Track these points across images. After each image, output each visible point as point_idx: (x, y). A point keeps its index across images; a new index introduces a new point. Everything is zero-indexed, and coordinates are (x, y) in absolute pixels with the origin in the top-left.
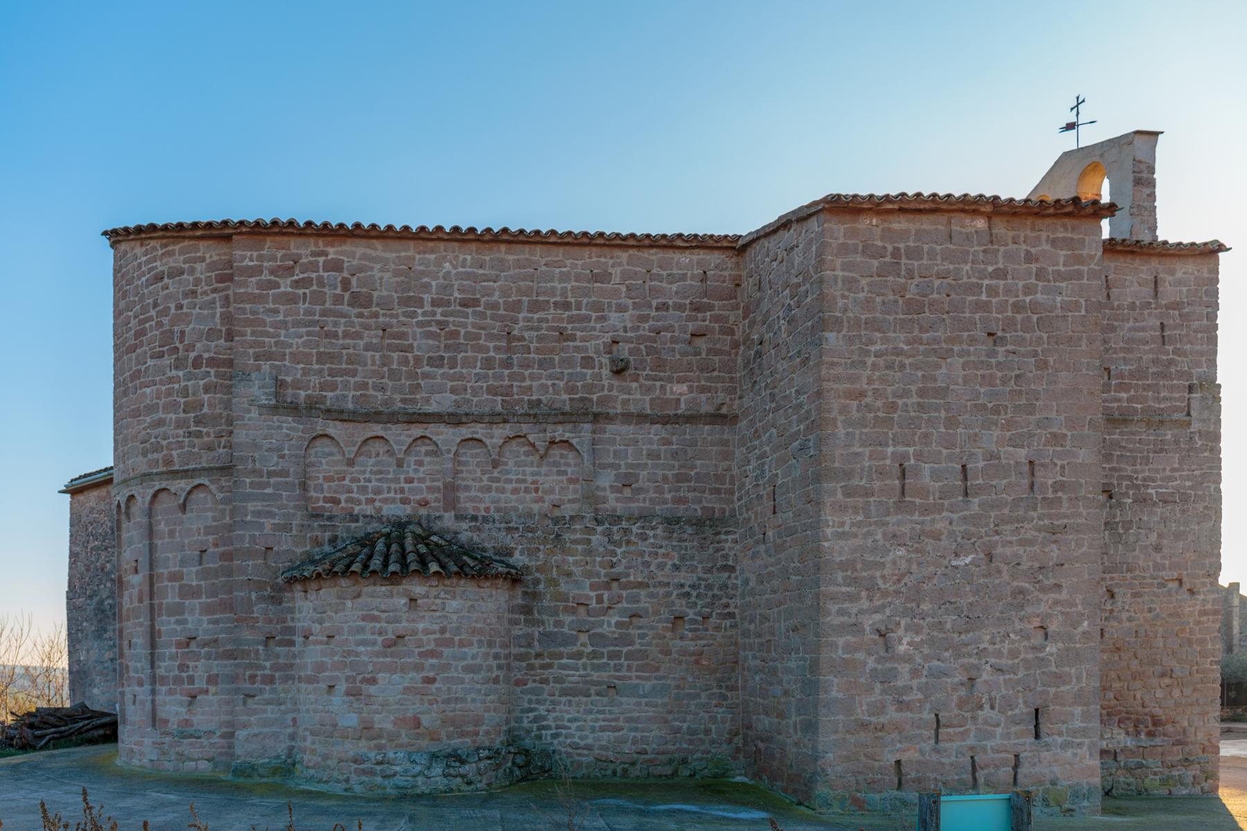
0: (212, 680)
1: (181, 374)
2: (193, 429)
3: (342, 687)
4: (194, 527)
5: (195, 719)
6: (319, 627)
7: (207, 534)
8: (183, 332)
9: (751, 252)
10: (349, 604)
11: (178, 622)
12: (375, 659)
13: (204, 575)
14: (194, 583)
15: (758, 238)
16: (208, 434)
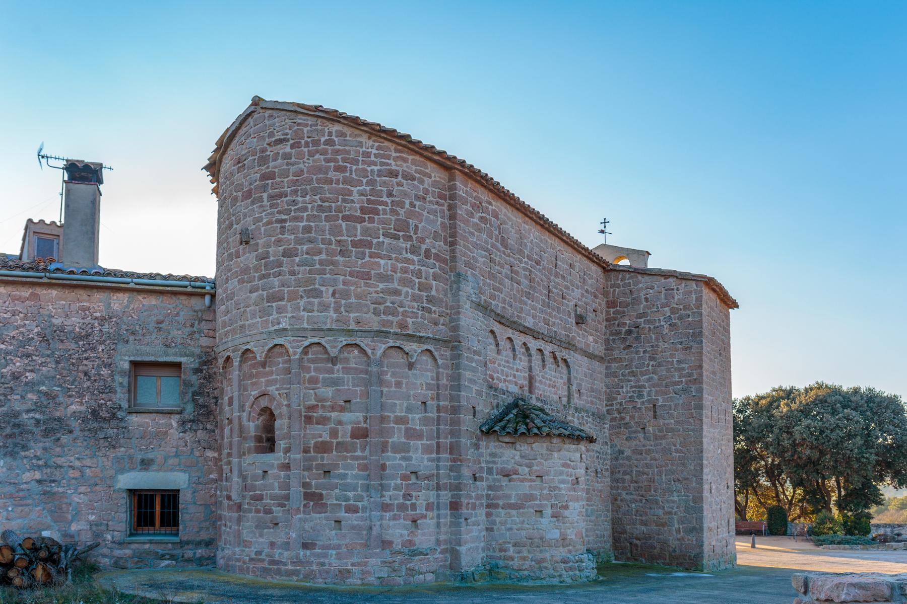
0: (429, 507)
1: (416, 258)
2: (425, 305)
3: (548, 511)
4: (418, 382)
5: (417, 540)
6: (527, 470)
7: (428, 389)
8: (416, 226)
9: (612, 274)
11: (404, 458)
13: (425, 421)
14: (418, 428)
15: (238, 129)
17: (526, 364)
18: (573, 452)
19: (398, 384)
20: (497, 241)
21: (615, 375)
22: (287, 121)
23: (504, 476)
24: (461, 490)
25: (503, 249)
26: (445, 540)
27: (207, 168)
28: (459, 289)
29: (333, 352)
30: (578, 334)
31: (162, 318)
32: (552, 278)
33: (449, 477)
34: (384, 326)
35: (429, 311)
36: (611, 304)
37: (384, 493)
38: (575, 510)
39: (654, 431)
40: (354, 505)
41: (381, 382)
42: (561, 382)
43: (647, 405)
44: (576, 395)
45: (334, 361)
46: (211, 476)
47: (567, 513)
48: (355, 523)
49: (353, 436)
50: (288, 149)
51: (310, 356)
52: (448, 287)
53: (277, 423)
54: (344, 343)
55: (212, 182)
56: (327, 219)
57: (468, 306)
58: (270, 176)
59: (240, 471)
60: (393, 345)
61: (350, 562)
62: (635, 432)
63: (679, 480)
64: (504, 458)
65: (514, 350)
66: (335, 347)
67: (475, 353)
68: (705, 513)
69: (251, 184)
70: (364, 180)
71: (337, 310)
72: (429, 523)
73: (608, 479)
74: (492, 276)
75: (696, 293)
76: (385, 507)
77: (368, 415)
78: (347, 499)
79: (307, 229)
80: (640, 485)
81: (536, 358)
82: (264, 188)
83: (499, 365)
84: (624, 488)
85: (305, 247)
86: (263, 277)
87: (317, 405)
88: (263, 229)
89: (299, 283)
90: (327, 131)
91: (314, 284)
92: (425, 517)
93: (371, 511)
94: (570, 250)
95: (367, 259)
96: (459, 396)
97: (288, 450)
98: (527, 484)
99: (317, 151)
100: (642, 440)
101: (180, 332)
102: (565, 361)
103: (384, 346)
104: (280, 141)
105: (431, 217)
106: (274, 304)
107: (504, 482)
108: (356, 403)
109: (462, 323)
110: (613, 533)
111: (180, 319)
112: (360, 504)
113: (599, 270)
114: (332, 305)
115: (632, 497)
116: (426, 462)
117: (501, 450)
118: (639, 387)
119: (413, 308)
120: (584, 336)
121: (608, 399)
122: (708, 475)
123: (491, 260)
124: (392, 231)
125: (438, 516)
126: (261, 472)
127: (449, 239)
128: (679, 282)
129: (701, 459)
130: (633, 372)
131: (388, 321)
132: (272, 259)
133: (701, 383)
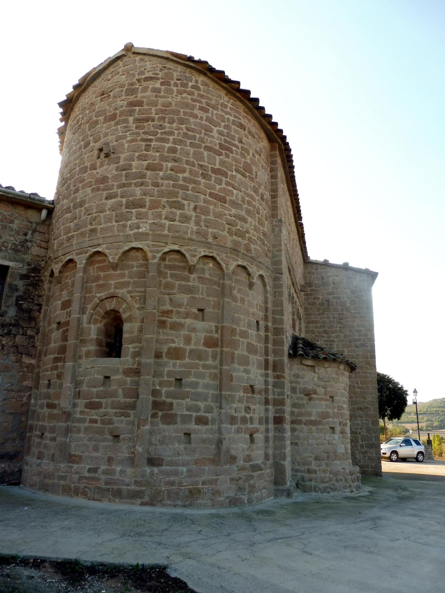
9: (309, 265)
22: (158, 65)
23: (305, 395)
27: (62, 104)
29: (193, 261)
45: (191, 269)
46: (25, 383)
48: (204, 436)
50: (158, 85)
51: (167, 262)
53: (126, 327)
54: (203, 254)
55: (61, 120)
56: (192, 145)
58: (139, 103)
59: (74, 376)
63: (361, 408)
64: (306, 379)
66: (195, 256)
69: (116, 109)
70: (223, 124)
71: (197, 223)
77: (219, 325)
78: (198, 410)
79: (173, 150)
82: (131, 113)
85: (170, 165)
87: (172, 311)
89: (162, 194)
90: (194, 79)
91: (177, 197)
98: (324, 403)
99: (185, 92)
101: (12, 238)
104: (151, 78)
111: (14, 226)
117: (303, 372)
124: (241, 169)
126: (101, 377)
130: (326, 330)
132: (134, 171)
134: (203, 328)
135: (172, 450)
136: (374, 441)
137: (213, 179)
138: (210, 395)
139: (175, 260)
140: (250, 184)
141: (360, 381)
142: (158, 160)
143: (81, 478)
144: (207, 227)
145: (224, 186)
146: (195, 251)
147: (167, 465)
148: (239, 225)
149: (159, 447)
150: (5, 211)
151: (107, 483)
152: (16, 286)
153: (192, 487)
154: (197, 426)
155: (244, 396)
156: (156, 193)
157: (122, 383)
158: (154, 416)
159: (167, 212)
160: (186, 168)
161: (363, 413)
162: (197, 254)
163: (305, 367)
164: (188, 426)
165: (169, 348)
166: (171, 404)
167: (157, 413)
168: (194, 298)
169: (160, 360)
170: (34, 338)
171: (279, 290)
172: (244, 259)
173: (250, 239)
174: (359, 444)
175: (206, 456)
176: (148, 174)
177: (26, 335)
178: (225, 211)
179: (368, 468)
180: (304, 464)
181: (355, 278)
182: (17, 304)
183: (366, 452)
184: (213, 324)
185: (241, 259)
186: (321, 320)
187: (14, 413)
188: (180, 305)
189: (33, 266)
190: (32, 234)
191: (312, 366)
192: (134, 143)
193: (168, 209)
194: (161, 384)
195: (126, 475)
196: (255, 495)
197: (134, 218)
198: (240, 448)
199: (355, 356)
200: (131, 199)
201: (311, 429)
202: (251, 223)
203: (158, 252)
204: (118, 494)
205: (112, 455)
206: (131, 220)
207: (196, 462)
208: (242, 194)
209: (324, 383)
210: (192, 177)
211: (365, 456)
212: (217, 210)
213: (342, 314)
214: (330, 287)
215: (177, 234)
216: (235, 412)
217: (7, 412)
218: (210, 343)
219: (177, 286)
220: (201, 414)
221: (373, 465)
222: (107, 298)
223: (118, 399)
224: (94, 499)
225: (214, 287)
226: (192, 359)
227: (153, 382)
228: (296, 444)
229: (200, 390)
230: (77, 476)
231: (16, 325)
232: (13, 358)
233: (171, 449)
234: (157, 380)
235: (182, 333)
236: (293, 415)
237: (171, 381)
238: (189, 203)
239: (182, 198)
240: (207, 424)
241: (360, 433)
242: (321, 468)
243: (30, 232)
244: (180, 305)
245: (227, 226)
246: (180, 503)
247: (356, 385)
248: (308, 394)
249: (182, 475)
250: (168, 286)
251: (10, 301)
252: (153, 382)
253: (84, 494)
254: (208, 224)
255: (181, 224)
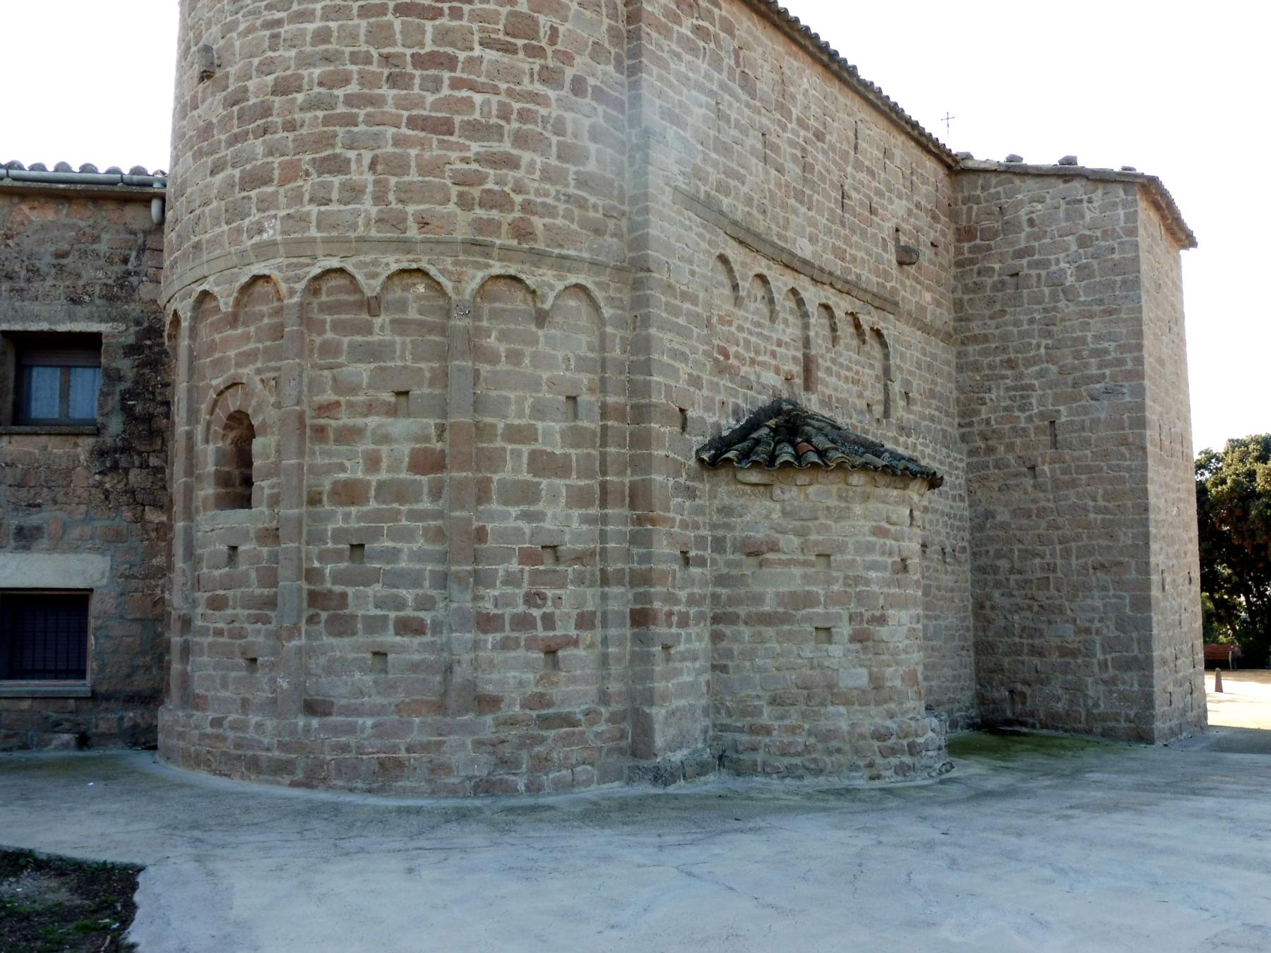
0: (584, 621)
1: (552, 94)
2: (572, 190)
5: (555, 693)
7: (579, 369)
8: (554, 31)
9: (965, 179)
10: (858, 509)
11: (525, 516)
12: (886, 590)
13: (575, 437)
14: (558, 452)
15: (985, 171)
16: (595, 206)
17: (798, 332)
18: (899, 505)
19: (515, 357)
20: (731, 75)
21: (976, 367)
23: (749, 555)
24: (651, 586)
25: (745, 97)
26: (620, 694)
28: (646, 160)
29: (371, 287)
30: (903, 284)
31: (67, 247)
32: (849, 169)
33: (628, 556)
34: (480, 230)
35: (582, 204)
36: (965, 234)
37: (482, 591)
38: (901, 626)
39: (1053, 471)
40: (415, 619)
41: (478, 353)
42: (869, 375)
43: (1037, 422)
44: (902, 403)
45: (372, 306)
46: (154, 561)
47: (883, 632)
48: (417, 657)
49: (415, 467)
51: (324, 298)
52: (625, 159)
53: (257, 444)
54: (394, 267)
57: (667, 198)
60: (502, 272)
61: (402, 743)
62: (1016, 475)
63: (1103, 566)
64: (748, 518)
65: (771, 301)
66: (374, 276)
67: (685, 296)
68: (1155, 632)
71: (379, 199)
72: (580, 658)
73: (968, 567)
74: (725, 149)
75: (1124, 207)
76: (486, 623)
78: (400, 604)
79: (322, 36)
80: (1029, 576)
81: (817, 321)
83: (740, 328)
84: (998, 584)
85: (317, 72)
86: (235, 139)
87: (338, 404)
88: (237, 44)
91: (333, 146)
92: (575, 643)
93: (452, 630)
94: (883, 123)
95: (446, 91)
96: (647, 384)
97: (275, 501)
98: (797, 571)
100: (1030, 489)
101: (100, 274)
102: (878, 334)
103: (480, 275)
105: (588, 13)
106: (253, 193)
107: (748, 567)
108: (421, 396)
109: (653, 231)
110: (978, 670)
111: (102, 247)
112: (427, 617)
113: (941, 172)
114: (370, 188)
115: (1012, 600)
116: (575, 525)
117: (742, 501)
118: (1023, 388)
119: (546, 195)
120: (914, 292)
121: (963, 415)
122: (1158, 556)
123: (720, 115)
124: (501, 36)
125: (605, 642)
126: (224, 548)
127: (627, 62)
128: (1090, 186)
129: (1145, 523)
131: (490, 221)
132: (252, 101)
133: (1141, 376)
134: (407, 433)
135: (351, 684)
136: (1136, 652)
137: (417, 81)
138: (427, 574)
139: (339, 289)
140: (526, 67)
141: (1101, 492)
142: (293, 66)
143: (204, 736)
144: (401, 201)
145: (446, 91)
146: (375, 263)
147: (340, 714)
148: (491, 178)
149: (323, 680)
150: (81, 219)
151: (238, 746)
152: (118, 370)
153: (383, 755)
154: (398, 638)
155: (522, 571)
156: (291, 145)
157: (254, 558)
158: (312, 620)
159: (313, 185)
160: (351, 72)
161: (1108, 578)
162: (379, 270)
163: (747, 488)
164: (379, 639)
165: (335, 483)
166: (344, 596)
167: (318, 615)
168: (382, 369)
169: (318, 509)
170: (164, 472)
171: (643, 311)
172: (510, 260)
173: (527, 207)
174: (1095, 661)
175: (419, 697)
176: (276, 105)
177: (148, 467)
178: (449, 153)
179: (1118, 721)
180: (744, 713)
181: (1090, 201)
182: (127, 410)
183: (1113, 681)
184: (431, 422)
185: (500, 260)
186: (997, 332)
187: (141, 620)
188: (354, 389)
189: (146, 325)
190: (138, 257)
191: (765, 485)
192: (250, 37)
193: (314, 178)
194: (323, 557)
195: (264, 730)
196: (551, 776)
197: (254, 210)
198: (511, 681)
199: (1087, 424)
200: (248, 167)
201: (760, 634)
202: (532, 165)
203: (298, 279)
204: (254, 766)
205: (247, 696)
206: (249, 215)
207: (399, 709)
208: (503, 98)
209: (798, 523)
210: (366, 91)
211: (1111, 692)
212: (427, 155)
213: (1054, 309)
214: (1023, 235)
215: (335, 234)
216: (496, 606)
217: (129, 617)
218: (428, 462)
219: (345, 346)
220: (409, 612)
221: (1132, 713)
222: (228, 388)
223: (250, 590)
224: (221, 774)
225: (429, 338)
226: (384, 502)
227: (308, 553)
228: (724, 669)
229: (403, 565)
230: (197, 732)
231: (127, 449)
232: (128, 514)
233: (346, 683)
234: (314, 549)
235: (361, 448)
236: (718, 603)
237: (342, 550)
238: (359, 155)
239: (343, 147)
240: (424, 633)
241: (1098, 632)
242: (787, 722)
243: (134, 254)
244: (354, 389)
245: (454, 190)
246: (360, 785)
247: (1091, 504)
248: (754, 552)
249: (362, 732)
250: (329, 349)
251: (110, 403)
252: (308, 553)
253: (208, 764)
254: (403, 196)
255: (342, 207)
